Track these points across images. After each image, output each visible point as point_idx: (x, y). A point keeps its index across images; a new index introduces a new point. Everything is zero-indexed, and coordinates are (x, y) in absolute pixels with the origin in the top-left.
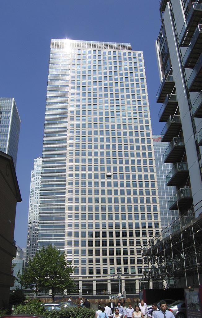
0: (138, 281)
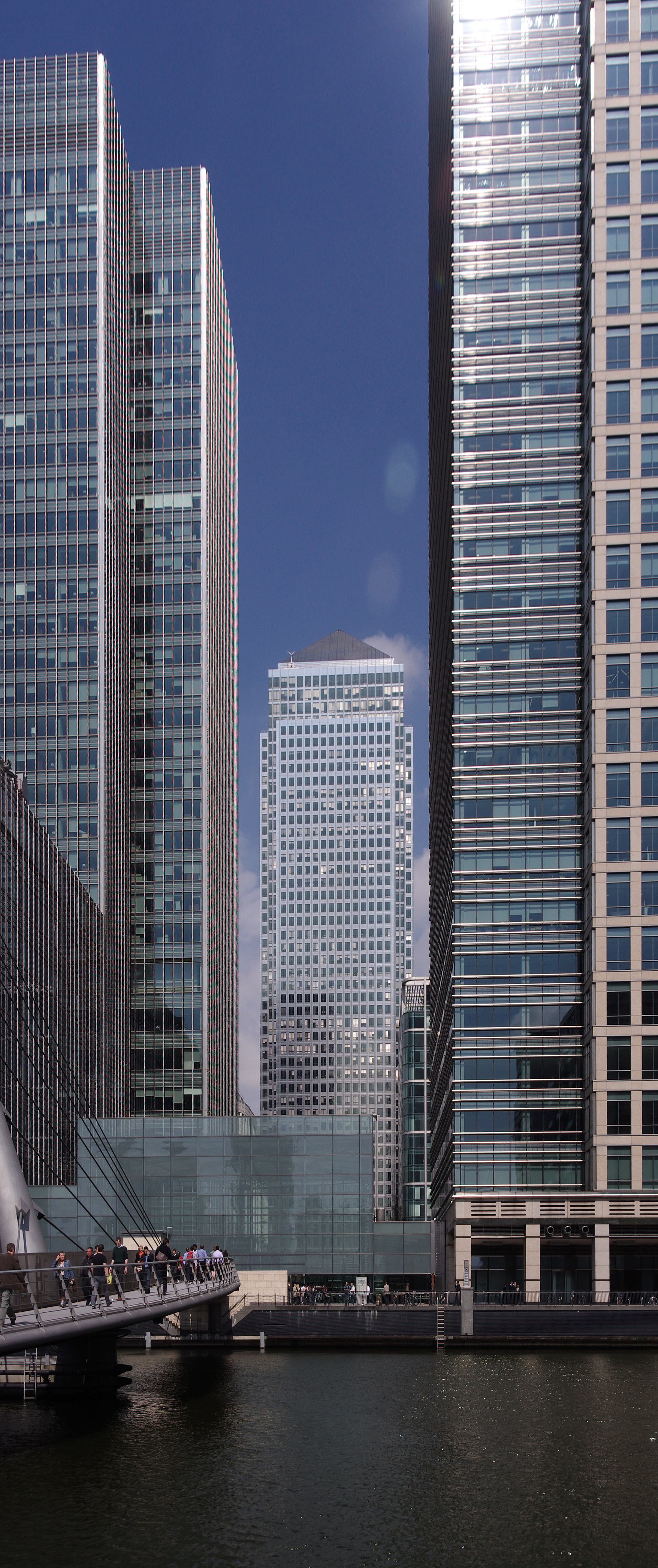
0: (469, 1233)
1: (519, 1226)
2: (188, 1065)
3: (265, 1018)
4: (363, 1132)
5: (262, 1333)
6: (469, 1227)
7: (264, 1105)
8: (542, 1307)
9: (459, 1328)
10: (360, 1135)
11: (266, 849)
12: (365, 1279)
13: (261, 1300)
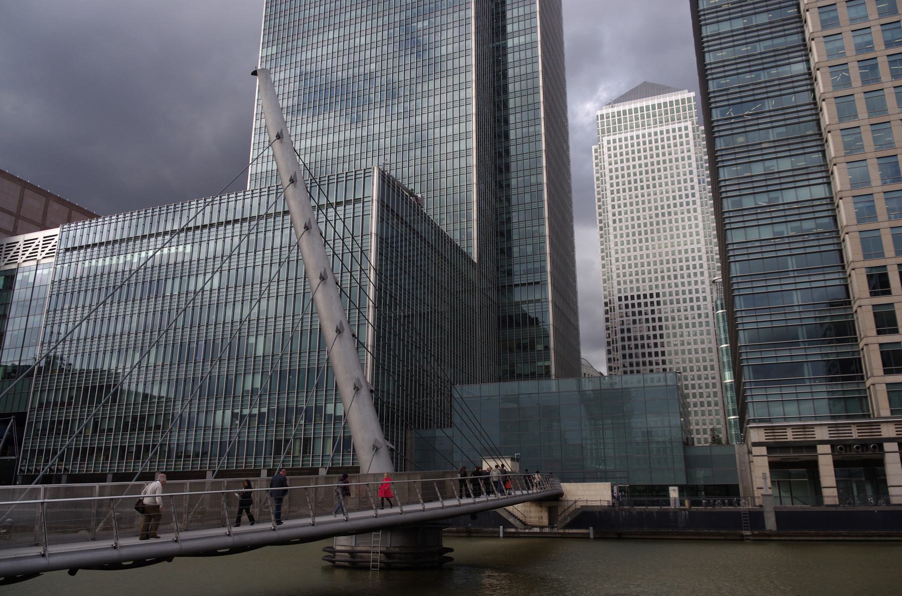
1: (812, 446)
2: (540, 347)
3: (607, 312)
4: (669, 383)
5: (591, 528)
6: (765, 448)
7: (610, 369)
8: (840, 509)
9: (763, 526)
10: (666, 386)
11: (601, 210)
12: (676, 488)
13: (589, 504)
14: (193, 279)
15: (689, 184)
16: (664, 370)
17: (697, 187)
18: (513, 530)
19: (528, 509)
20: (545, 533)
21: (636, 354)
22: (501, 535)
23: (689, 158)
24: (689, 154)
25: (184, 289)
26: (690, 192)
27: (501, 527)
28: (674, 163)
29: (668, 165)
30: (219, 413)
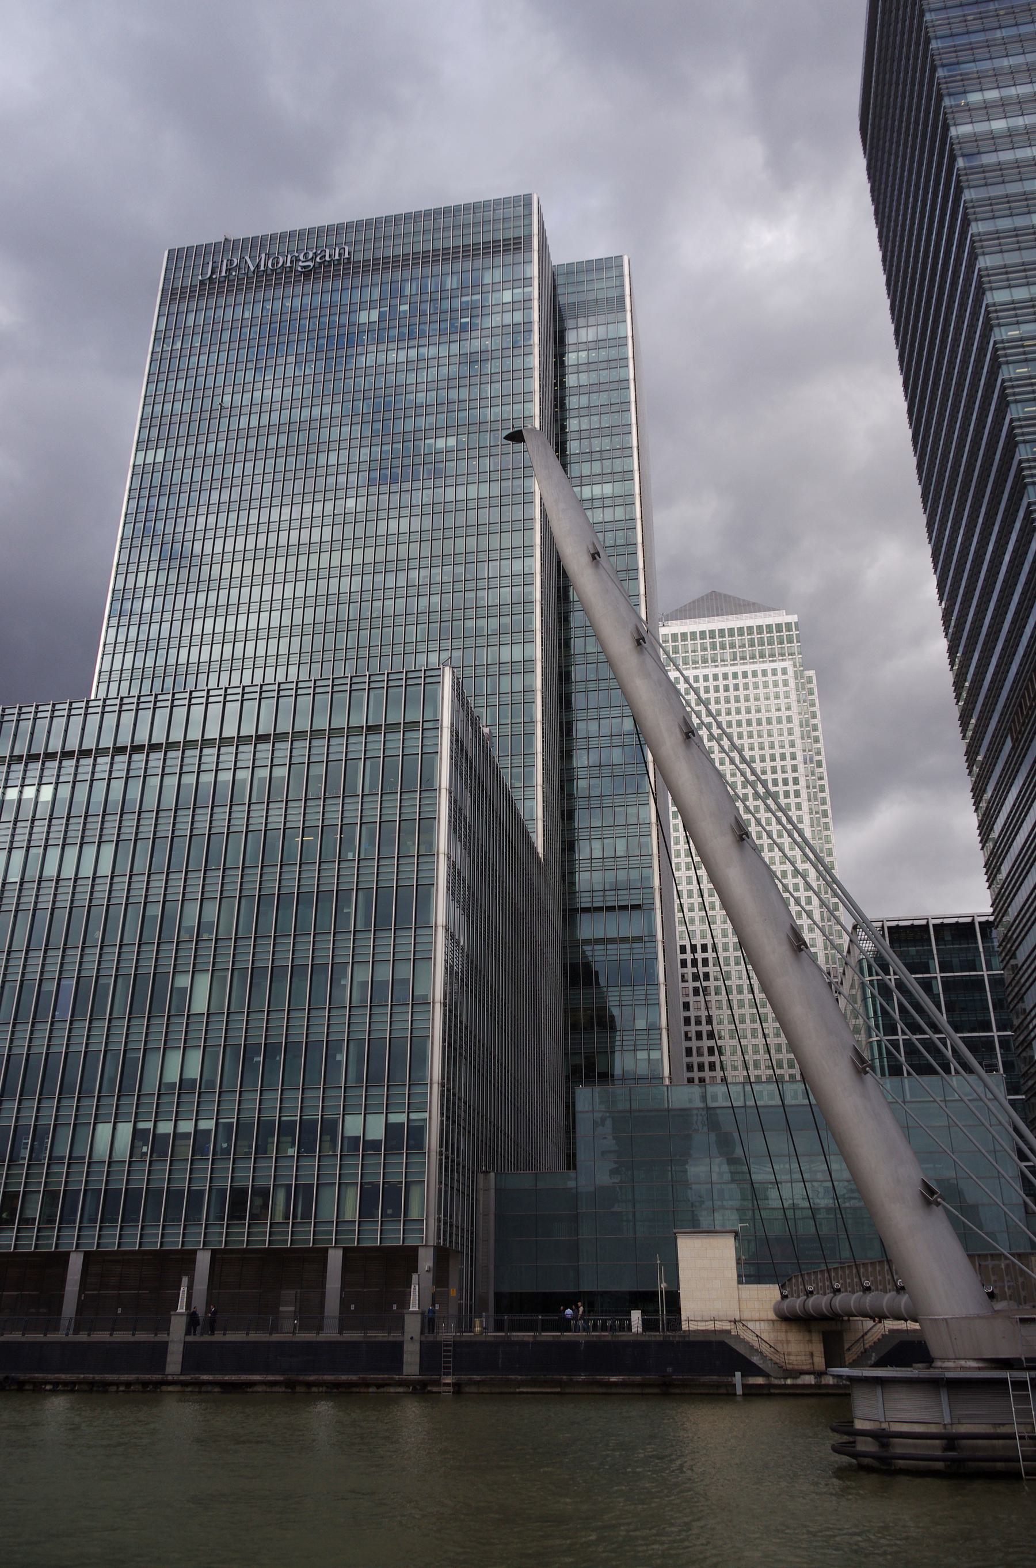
8: (643, 1339)
14: (54, 854)
15: (789, 763)
16: (702, 1080)
17: (801, 768)
18: (760, 1380)
19: (782, 1336)
20: (827, 1386)
21: (699, 1049)
22: (739, 1391)
23: (789, 720)
24: (788, 713)
25: (33, 873)
26: (790, 775)
27: (738, 1374)
28: (765, 727)
29: (754, 728)
30: (104, 1130)
